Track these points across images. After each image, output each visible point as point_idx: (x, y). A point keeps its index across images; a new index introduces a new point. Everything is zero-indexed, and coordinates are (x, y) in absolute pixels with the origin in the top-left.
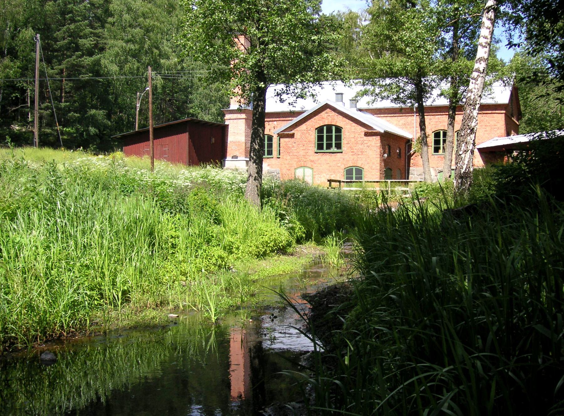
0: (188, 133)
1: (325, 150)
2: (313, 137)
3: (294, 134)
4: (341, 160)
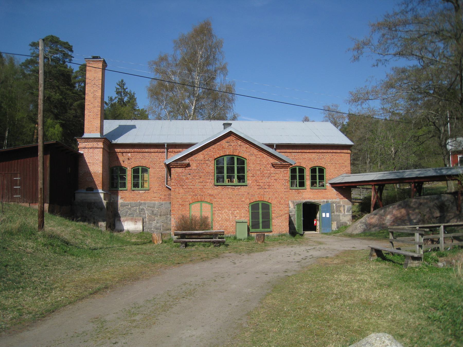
4: (246, 194)
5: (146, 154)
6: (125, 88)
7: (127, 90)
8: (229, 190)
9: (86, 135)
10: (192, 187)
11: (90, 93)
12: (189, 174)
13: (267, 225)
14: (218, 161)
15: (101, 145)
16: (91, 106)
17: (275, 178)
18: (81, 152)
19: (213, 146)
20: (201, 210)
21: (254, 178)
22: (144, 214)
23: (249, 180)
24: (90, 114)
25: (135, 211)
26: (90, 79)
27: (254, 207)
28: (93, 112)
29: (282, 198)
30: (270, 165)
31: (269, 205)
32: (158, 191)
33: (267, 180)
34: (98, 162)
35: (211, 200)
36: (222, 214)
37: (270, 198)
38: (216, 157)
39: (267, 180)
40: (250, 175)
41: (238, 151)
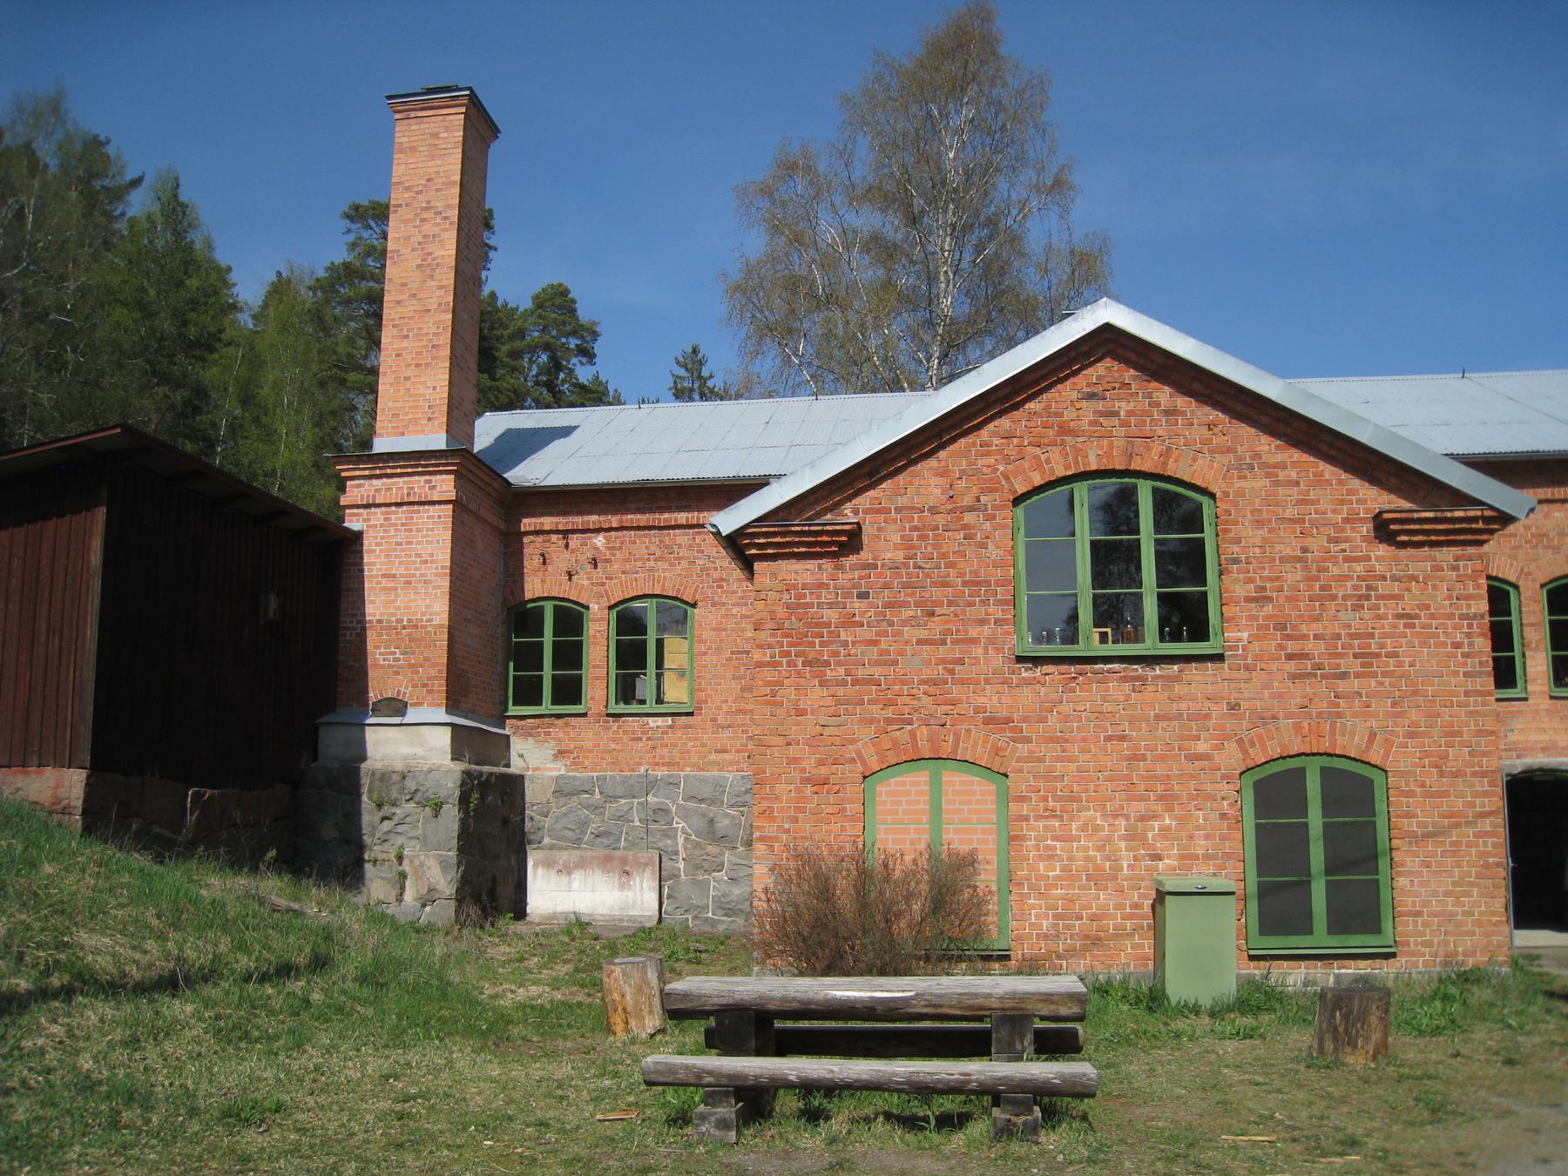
0: (101, 513)
1: (1151, 644)
5: (682, 537)
6: (705, 373)
7: (710, 383)
8: (1110, 691)
10: (877, 672)
11: (405, 251)
12: (863, 596)
13: (1360, 910)
15: (445, 486)
16: (411, 307)
17: (1408, 604)
18: (353, 523)
19: (1004, 423)
20: (936, 810)
21: (1269, 609)
22: (670, 834)
23: (1234, 626)
24: (405, 343)
25: (624, 818)
26: (408, 189)
27: (1275, 791)
28: (419, 336)
29: (1452, 733)
30: (1366, 529)
31: (1369, 783)
32: (739, 718)
33: (1354, 621)
34: (429, 571)
35: (997, 751)
36: (1071, 839)
37: (1372, 736)
38: (1021, 488)
39: (1354, 621)
40: (1241, 590)
41: (1157, 448)
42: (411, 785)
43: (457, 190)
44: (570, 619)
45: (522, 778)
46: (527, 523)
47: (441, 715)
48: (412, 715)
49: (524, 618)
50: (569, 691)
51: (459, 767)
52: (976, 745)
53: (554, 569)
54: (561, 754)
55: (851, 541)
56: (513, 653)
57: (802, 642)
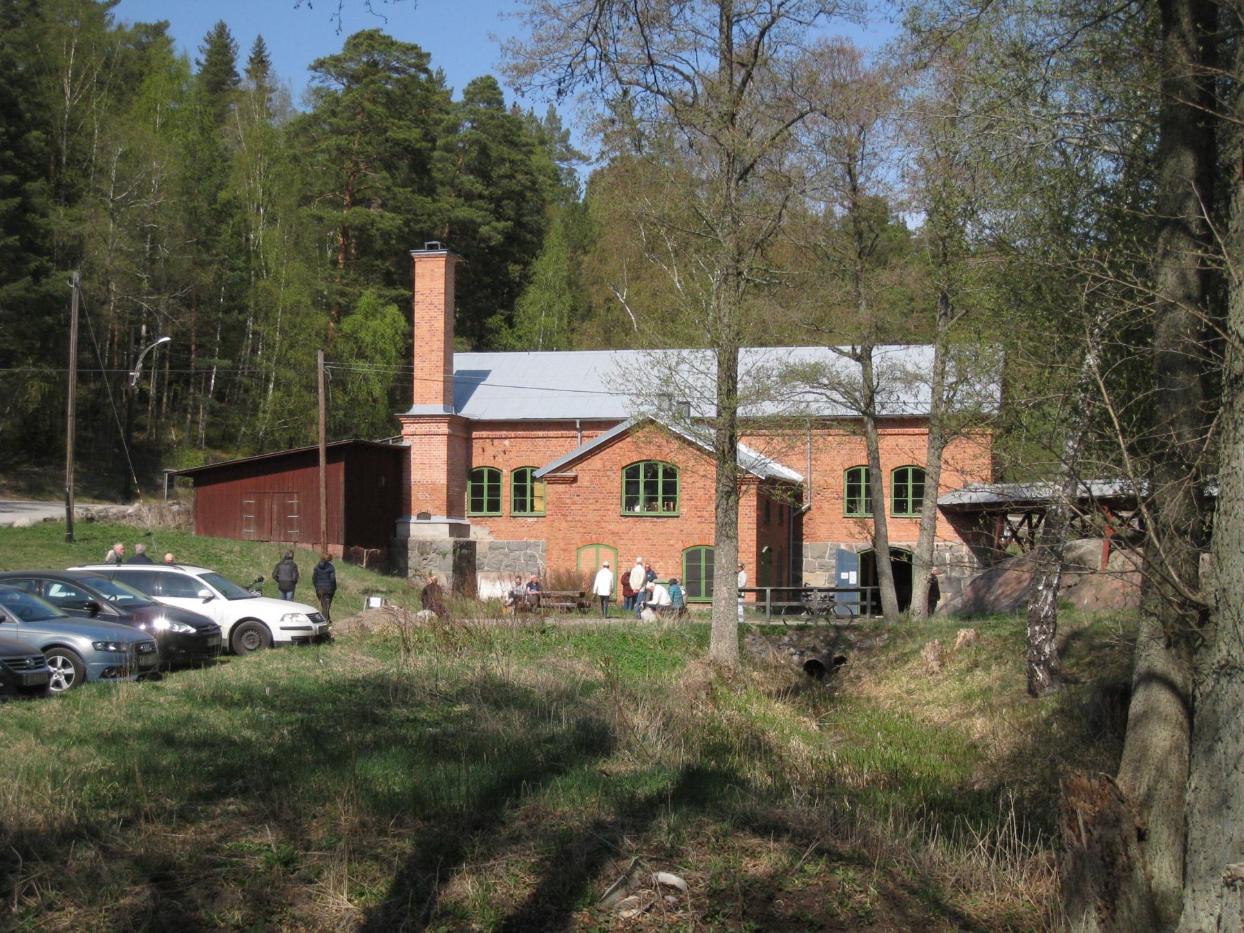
0: (342, 464)
1: (660, 512)
2: (616, 484)
3: (896, 552)
4: (677, 532)
5: (541, 442)
8: (647, 525)
9: (416, 409)
14: (632, 472)
15: (444, 428)
16: (426, 348)
19: (620, 444)
23: (683, 506)
25: (518, 559)
42: (434, 546)
43: (443, 297)
44: (495, 476)
45: (474, 543)
46: (475, 434)
47: (444, 519)
48: (433, 519)
49: (476, 476)
50: (494, 506)
51: (452, 539)
52: (609, 540)
53: (485, 455)
54: (491, 532)
55: (574, 480)
56: (475, 488)
57: (560, 507)
